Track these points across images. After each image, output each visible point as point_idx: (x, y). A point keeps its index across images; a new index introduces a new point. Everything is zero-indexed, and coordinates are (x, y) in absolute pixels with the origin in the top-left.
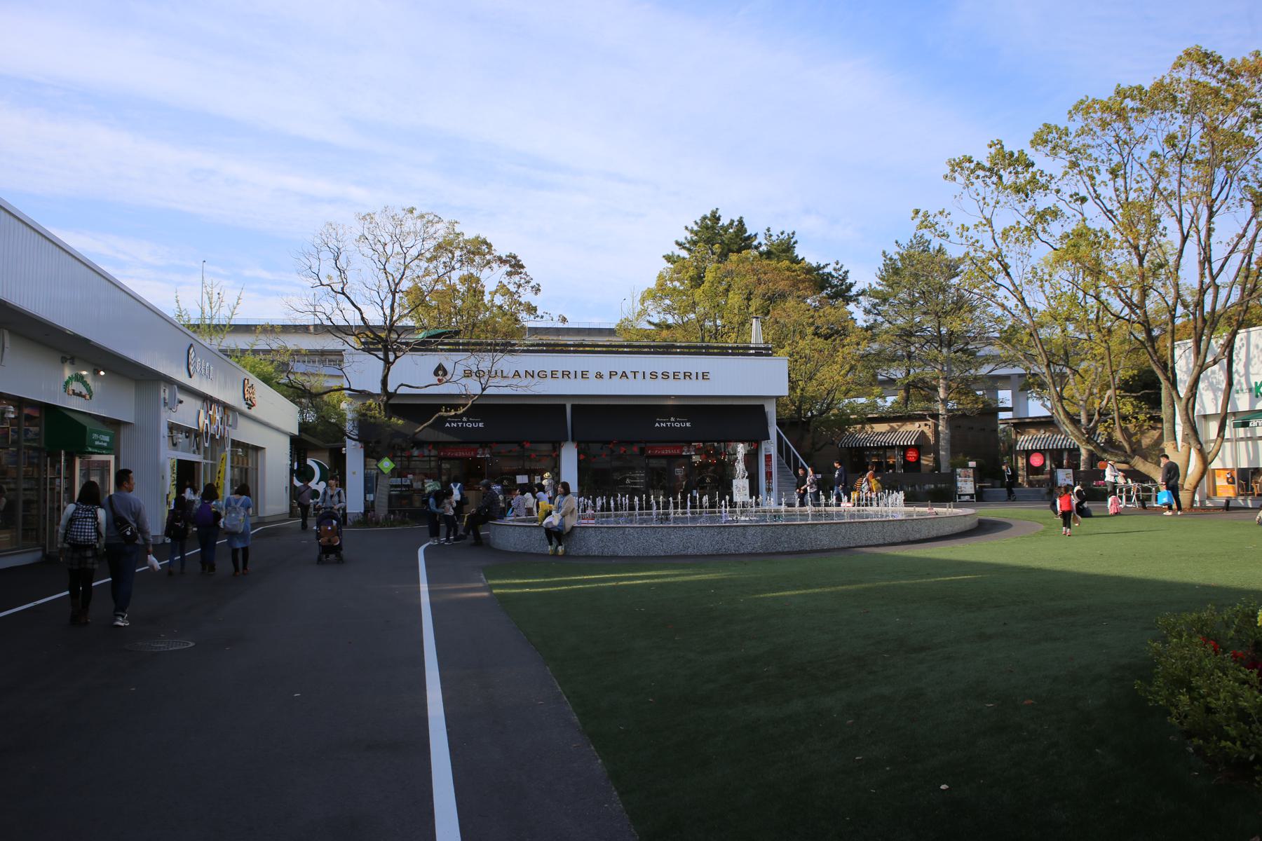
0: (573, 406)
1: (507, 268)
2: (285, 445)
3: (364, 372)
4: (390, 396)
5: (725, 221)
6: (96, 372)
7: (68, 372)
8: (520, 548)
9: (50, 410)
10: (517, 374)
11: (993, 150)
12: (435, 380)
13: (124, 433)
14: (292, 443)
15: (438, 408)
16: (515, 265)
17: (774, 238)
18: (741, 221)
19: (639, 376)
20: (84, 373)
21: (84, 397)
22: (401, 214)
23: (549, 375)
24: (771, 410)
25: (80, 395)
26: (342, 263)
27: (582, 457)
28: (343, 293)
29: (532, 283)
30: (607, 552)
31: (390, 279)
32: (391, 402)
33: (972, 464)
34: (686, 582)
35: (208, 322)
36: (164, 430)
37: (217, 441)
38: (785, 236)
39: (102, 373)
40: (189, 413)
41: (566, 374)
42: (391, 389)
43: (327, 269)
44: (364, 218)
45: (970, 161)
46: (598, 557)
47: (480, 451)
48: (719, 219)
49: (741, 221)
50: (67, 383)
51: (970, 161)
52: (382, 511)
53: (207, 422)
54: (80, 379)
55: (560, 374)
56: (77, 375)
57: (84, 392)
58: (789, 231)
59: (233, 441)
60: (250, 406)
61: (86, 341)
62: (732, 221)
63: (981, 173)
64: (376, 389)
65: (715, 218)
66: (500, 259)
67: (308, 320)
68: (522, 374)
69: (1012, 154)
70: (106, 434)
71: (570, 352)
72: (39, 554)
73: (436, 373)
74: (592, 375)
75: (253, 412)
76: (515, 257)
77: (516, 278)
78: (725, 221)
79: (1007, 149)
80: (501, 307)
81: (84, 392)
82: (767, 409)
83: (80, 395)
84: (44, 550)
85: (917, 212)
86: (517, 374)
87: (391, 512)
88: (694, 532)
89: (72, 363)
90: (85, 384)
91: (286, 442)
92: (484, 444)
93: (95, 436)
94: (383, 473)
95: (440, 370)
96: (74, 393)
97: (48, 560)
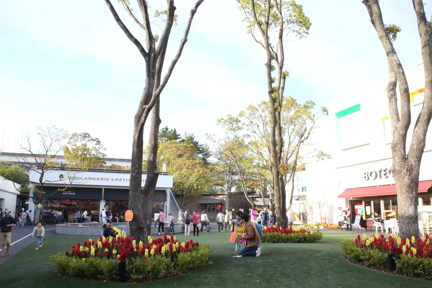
0: (105, 189)
1: (95, 142)
3: (34, 176)
4: (42, 184)
5: (170, 130)
8: (61, 233)
10: (86, 178)
11: (228, 117)
12: (59, 179)
14: (18, 197)
15: (57, 188)
16: (99, 142)
17: (187, 135)
18: (175, 130)
19: (125, 180)
23: (96, 179)
24: (168, 192)
29: (103, 148)
30: (83, 234)
31: (46, 147)
33: (233, 210)
38: (191, 135)
41: (102, 179)
42: (43, 182)
45: (223, 119)
46: (71, 235)
47: (74, 202)
48: (86, 146)
49: (175, 130)
51: (223, 119)
55: (100, 179)
58: (192, 133)
62: (172, 130)
63: (227, 123)
65: (167, 129)
66: (92, 140)
68: (88, 178)
69: (234, 118)
71: (104, 172)
73: (60, 177)
74: (110, 179)
76: (98, 139)
77: (98, 146)
78: (170, 130)
79: (232, 117)
80: (94, 155)
82: (167, 191)
85: (207, 134)
86: (86, 178)
88: (74, 228)
91: (16, 196)
92: (75, 200)
94: (38, 208)
95: (61, 176)
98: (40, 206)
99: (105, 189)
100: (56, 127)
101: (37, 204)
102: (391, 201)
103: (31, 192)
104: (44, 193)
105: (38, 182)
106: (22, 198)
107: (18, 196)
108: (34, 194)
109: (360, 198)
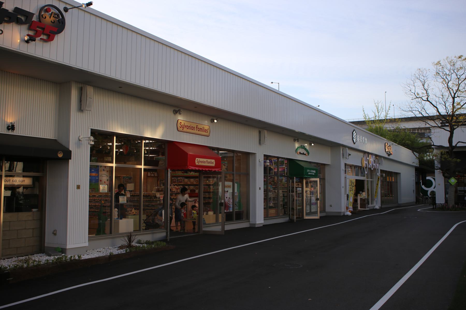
2: (412, 172)
3: (440, 138)
6: (310, 144)
7: (297, 145)
9: (291, 161)
13: (327, 169)
20: (306, 145)
21: (305, 154)
22: (455, 60)
25: (303, 154)
26: (426, 86)
27: (265, 207)
28: (428, 101)
31: (452, 92)
32: (454, 150)
34: (15, 305)
35: (377, 119)
36: (343, 167)
37: (372, 171)
39: (313, 144)
40: (355, 159)
42: (454, 144)
43: (420, 91)
44: (437, 64)
50: (297, 149)
52: (452, 203)
53: (367, 162)
54: (304, 148)
56: (301, 146)
57: (305, 152)
59: (381, 170)
60: (389, 155)
61: (304, 134)
64: (447, 145)
67: (411, 115)
70: (313, 169)
72: (288, 219)
75: (391, 157)
81: (305, 152)
83: (303, 154)
84: (290, 217)
87: (456, 203)
89: (298, 141)
90: (305, 149)
93: (308, 171)
94: (451, 185)
96: (300, 153)
97: (291, 221)
98: (453, 181)
99: (272, 164)
100: (463, 58)
101: (449, 178)
102: (115, 137)
103: (436, 162)
104: (459, 160)
105: (447, 145)
106: (423, 171)
107: (417, 169)
108: (441, 162)
109: (233, 151)
